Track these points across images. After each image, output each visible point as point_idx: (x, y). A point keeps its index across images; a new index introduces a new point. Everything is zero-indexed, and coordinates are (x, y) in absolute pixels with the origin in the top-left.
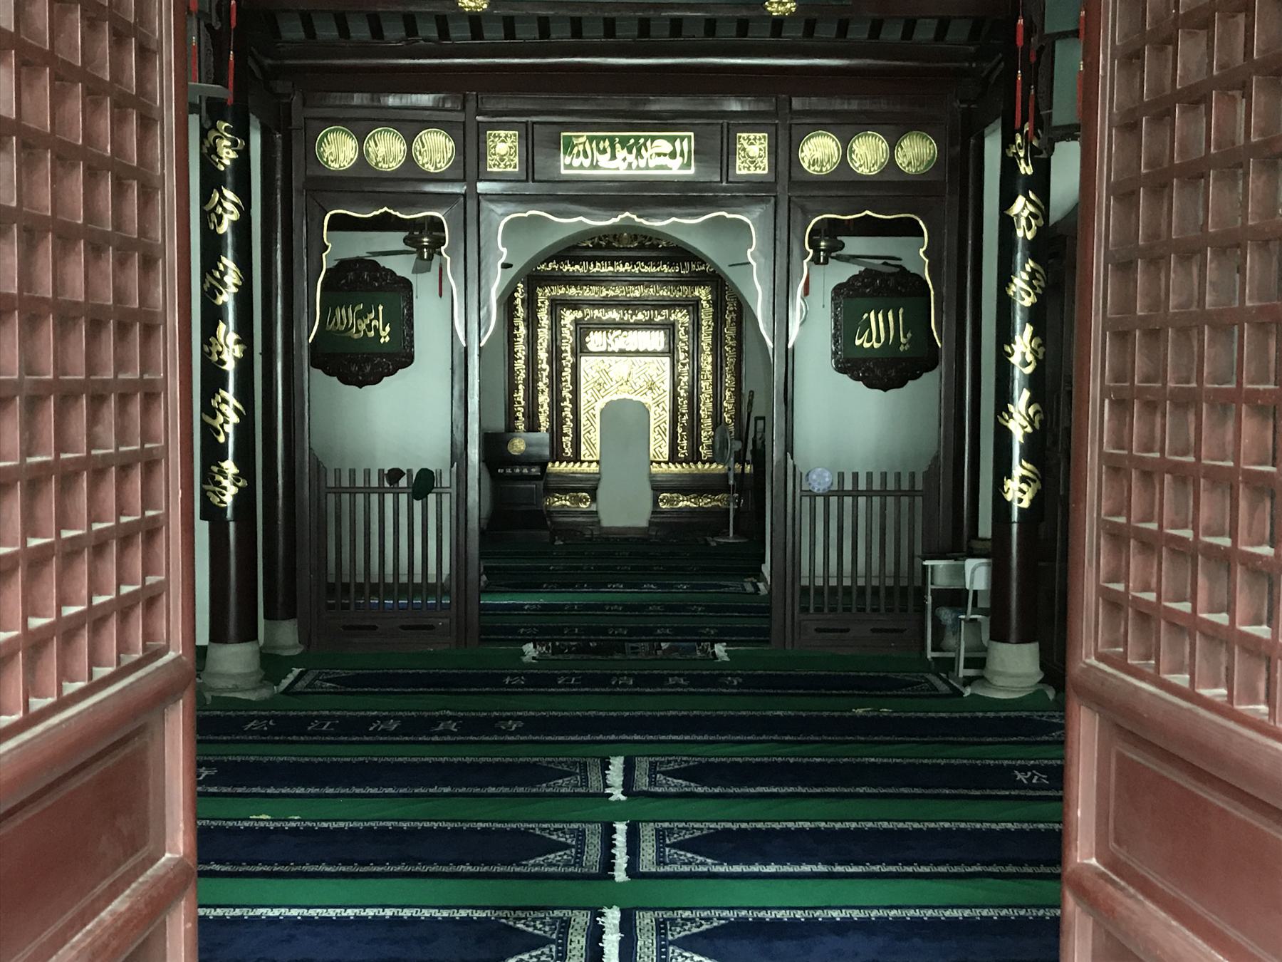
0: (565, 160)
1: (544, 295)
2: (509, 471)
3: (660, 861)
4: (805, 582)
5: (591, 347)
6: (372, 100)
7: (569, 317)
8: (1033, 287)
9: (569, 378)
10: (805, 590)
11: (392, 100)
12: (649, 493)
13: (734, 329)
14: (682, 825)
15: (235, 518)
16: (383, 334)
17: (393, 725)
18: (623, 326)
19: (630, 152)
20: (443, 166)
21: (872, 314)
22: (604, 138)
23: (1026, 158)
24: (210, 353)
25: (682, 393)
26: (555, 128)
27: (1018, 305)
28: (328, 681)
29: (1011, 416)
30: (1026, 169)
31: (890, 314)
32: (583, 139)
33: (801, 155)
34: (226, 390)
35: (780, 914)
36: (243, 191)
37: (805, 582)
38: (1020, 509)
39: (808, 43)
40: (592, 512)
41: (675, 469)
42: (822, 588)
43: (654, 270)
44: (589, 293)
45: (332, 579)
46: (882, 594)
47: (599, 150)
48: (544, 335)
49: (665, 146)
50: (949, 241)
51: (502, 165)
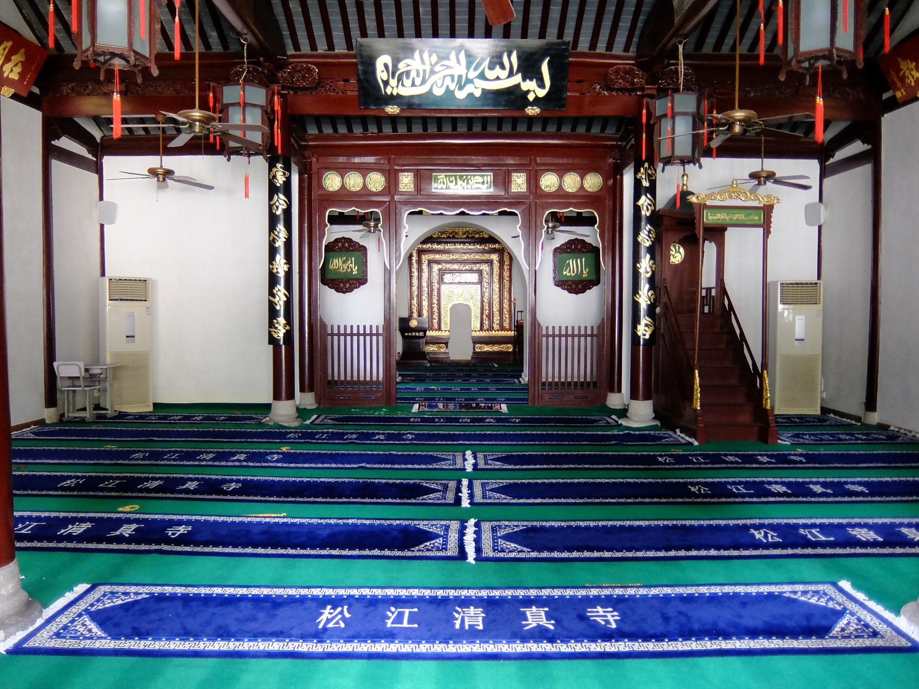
0: (434, 185)
1: (425, 258)
2: (410, 334)
3: (484, 497)
4: (544, 380)
5: (446, 280)
6: (348, 159)
7: (436, 267)
8: (650, 238)
9: (436, 294)
10: (544, 384)
11: (357, 160)
12: (472, 344)
13: (508, 273)
14: (494, 481)
15: (284, 343)
16: (354, 270)
17: (354, 436)
18: (460, 271)
19: (464, 181)
20: (380, 189)
21: (571, 260)
22: (452, 176)
23: (646, 179)
24: (273, 269)
25: (486, 301)
26: (428, 172)
27: (642, 246)
28: (329, 419)
29: (640, 296)
30: (646, 184)
31: (579, 260)
32: (442, 177)
33: (541, 183)
34: (280, 285)
35: (553, 524)
36: (288, 194)
37: (544, 380)
38: (644, 339)
39: (543, 133)
40: (446, 353)
41: (483, 334)
42: (551, 383)
43: (473, 247)
44: (445, 257)
45: (330, 378)
46: (579, 384)
47: (450, 181)
48: (425, 275)
49: (480, 179)
50: (608, 223)
51: (406, 188)
